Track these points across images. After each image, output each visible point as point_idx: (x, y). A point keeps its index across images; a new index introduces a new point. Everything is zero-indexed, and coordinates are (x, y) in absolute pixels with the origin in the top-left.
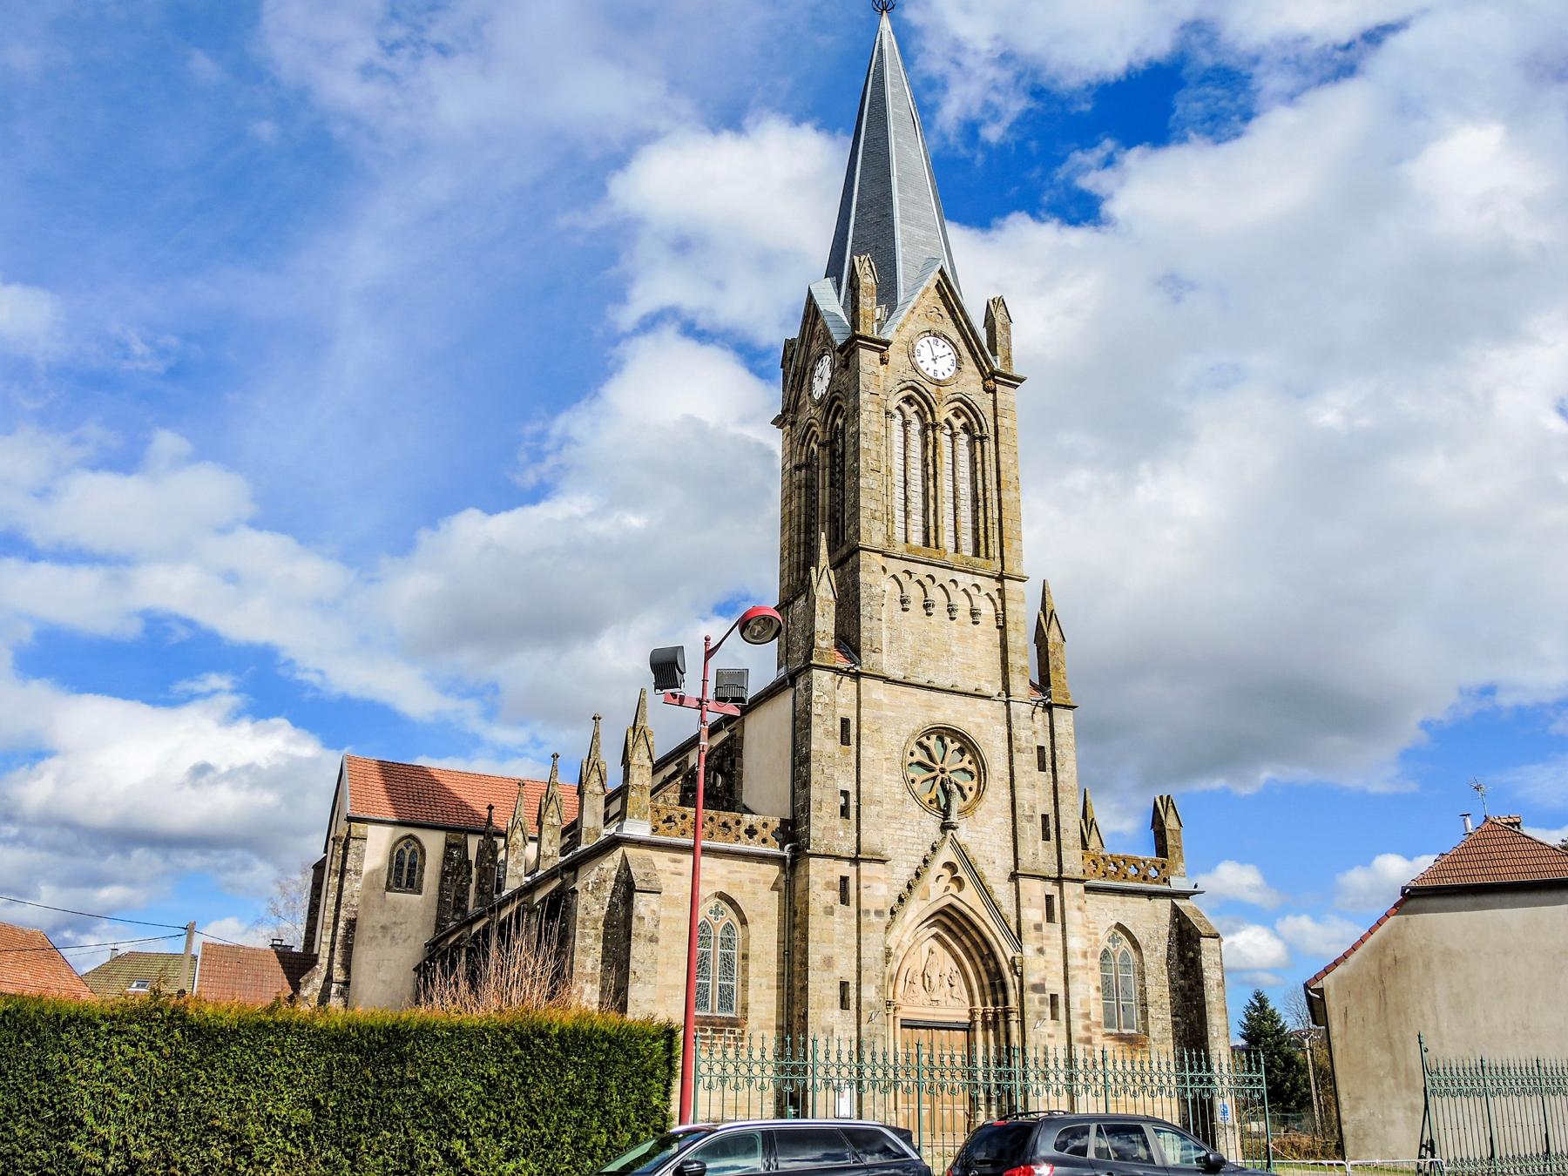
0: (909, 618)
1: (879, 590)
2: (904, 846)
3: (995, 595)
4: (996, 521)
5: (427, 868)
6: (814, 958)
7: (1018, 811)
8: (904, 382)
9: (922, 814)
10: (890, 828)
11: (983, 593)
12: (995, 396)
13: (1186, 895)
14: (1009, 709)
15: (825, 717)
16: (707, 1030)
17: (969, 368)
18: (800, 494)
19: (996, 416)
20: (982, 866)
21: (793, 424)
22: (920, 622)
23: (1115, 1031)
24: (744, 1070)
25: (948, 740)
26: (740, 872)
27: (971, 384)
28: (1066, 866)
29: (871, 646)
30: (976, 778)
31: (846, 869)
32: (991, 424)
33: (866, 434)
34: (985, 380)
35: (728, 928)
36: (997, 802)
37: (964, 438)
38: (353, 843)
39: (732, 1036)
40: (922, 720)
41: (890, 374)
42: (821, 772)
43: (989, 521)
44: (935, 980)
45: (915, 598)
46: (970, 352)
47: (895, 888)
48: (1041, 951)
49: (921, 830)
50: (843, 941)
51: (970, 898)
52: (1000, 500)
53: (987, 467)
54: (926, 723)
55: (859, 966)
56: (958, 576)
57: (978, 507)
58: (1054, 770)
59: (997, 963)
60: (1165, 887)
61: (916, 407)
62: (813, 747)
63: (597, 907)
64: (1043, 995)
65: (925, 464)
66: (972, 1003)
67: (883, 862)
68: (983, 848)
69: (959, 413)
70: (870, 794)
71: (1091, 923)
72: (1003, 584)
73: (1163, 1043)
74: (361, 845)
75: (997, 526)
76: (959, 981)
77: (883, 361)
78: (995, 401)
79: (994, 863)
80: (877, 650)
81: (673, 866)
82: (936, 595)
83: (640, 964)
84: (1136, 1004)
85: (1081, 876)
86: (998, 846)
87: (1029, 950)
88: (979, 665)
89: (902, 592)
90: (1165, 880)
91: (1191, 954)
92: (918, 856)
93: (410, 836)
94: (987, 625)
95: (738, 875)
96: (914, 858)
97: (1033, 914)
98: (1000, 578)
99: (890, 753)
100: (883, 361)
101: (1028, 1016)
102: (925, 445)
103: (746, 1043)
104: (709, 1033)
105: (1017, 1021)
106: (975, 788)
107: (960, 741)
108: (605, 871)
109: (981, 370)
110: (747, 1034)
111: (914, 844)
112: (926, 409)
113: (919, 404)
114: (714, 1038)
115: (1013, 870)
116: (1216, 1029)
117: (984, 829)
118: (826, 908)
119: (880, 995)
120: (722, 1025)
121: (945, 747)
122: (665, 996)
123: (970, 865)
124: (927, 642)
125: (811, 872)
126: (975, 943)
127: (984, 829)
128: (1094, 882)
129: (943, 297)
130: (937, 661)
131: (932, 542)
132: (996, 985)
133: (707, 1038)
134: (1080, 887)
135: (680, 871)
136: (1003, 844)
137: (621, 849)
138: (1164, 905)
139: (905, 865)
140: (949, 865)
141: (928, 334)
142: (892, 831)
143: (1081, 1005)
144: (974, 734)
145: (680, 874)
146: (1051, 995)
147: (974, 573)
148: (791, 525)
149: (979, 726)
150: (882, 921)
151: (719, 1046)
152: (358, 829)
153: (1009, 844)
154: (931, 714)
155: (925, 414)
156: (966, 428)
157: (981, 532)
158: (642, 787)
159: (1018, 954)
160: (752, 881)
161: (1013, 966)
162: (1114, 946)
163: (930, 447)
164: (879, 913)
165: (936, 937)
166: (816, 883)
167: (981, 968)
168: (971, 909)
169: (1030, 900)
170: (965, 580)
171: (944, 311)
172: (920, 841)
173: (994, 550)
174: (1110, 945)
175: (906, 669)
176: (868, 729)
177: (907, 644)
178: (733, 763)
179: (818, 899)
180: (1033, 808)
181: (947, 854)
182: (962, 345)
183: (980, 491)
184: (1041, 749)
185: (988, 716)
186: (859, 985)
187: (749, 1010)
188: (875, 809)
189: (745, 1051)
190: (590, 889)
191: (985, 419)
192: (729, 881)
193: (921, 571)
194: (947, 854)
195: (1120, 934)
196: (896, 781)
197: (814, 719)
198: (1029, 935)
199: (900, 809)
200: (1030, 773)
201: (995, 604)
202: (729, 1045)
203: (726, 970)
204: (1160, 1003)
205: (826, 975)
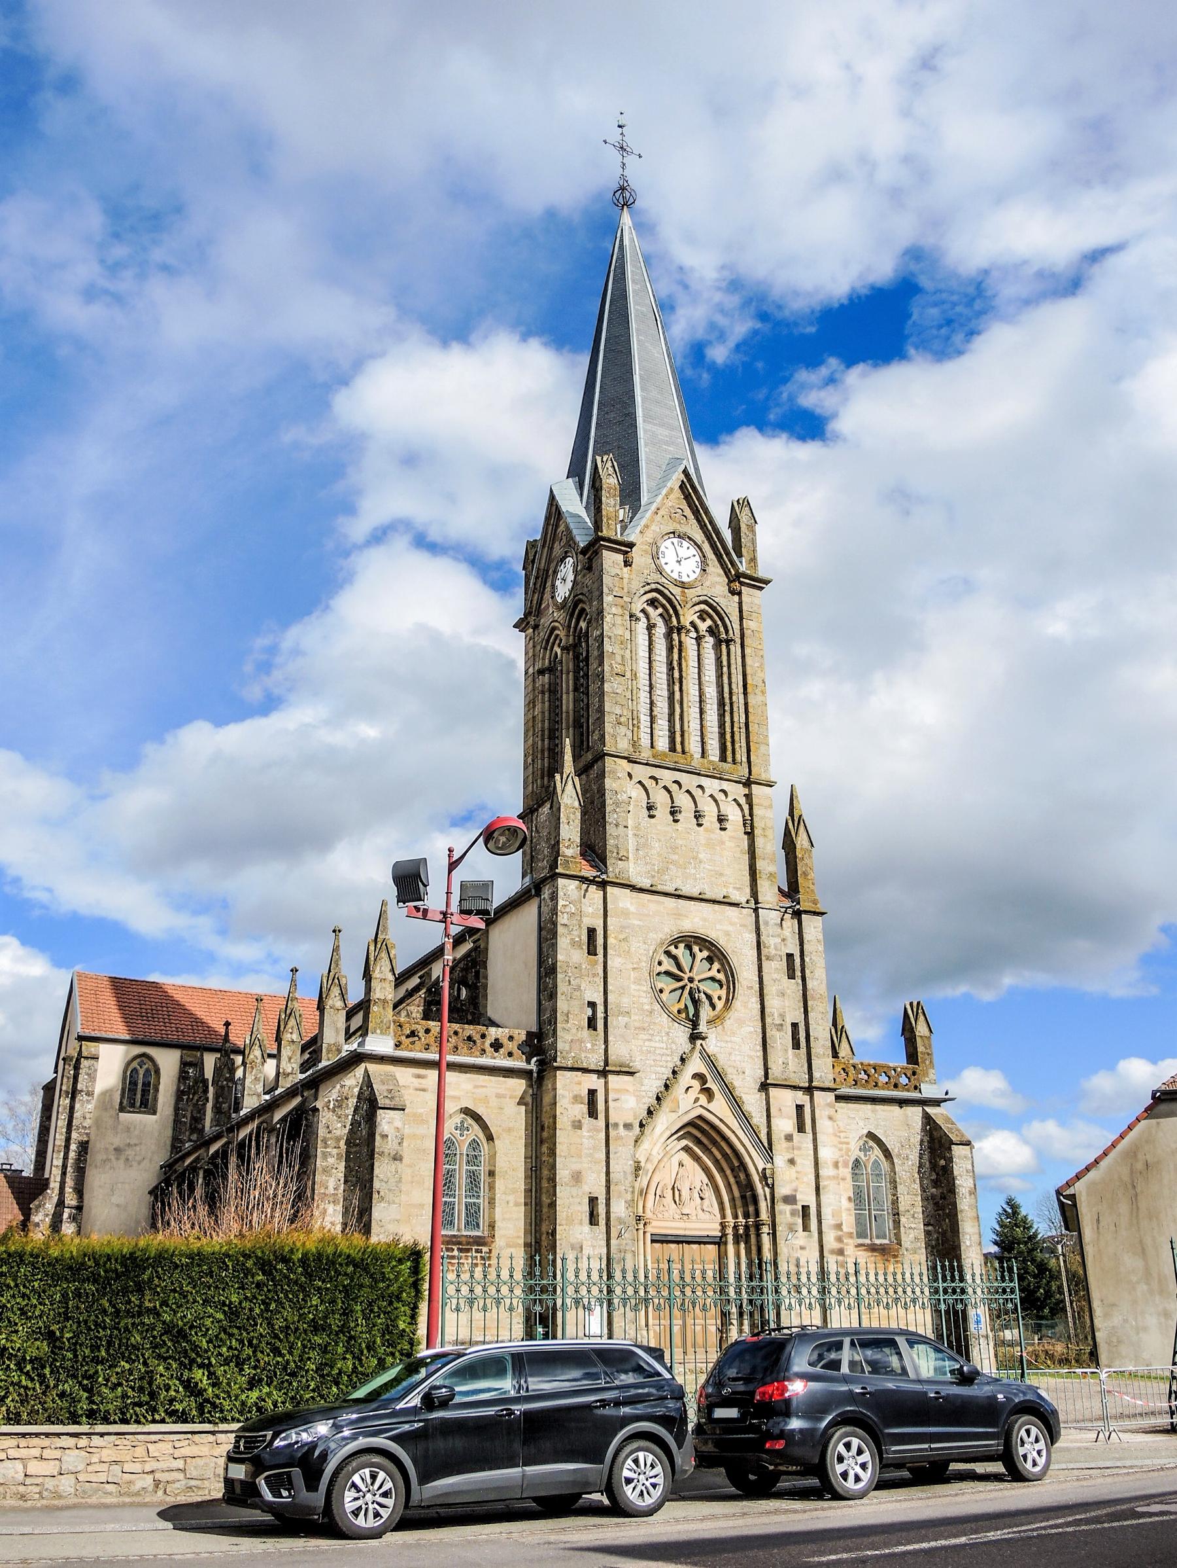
1: (625, 797)
2: (653, 1058)
3: (743, 801)
4: (743, 726)
5: (161, 1087)
6: (563, 1173)
7: (768, 1020)
8: (648, 584)
11: (730, 798)
12: (740, 598)
13: (937, 1102)
14: (757, 917)
18: (543, 699)
19: (741, 618)
20: (733, 1078)
21: (536, 627)
22: (669, 829)
25: (696, 949)
27: (716, 585)
28: (816, 1074)
30: (725, 987)
31: (594, 1082)
32: (736, 626)
33: (610, 638)
34: (730, 582)
35: (474, 1145)
37: (709, 641)
38: (84, 1063)
39: (479, 1255)
41: (633, 576)
43: (736, 725)
44: (685, 1193)
46: (715, 554)
48: (792, 1162)
50: (591, 1155)
51: (720, 1109)
52: (746, 704)
53: (733, 671)
55: (608, 1181)
56: (705, 782)
57: (724, 711)
58: (804, 979)
59: (748, 1175)
60: (915, 1095)
61: (660, 610)
62: (560, 957)
63: (339, 1125)
65: (671, 669)
66: (723, 1216)
67: (632, 1074)
68: (733, 1058)
69: (705, 616)
70: (618, 1006)
72: (750, 790)
74: (93, 1065)
75: (743, 730)
76: (709, 1194)
77: (627, 563)
78: (740, 603)
82: (683, 800)
83: (383, 1184)
84: (888, 1213)
85: (832, 1085)
87: (780, 1160)
88: (728, 871)
89: (649, 799)
90: (916, 1087)
91: (943, 1162)
93: (144, 1055)
97: (784, 1124)
98: (748, 783)
100: (627, 563)
101: (779, 1228)
102: (670, 649)
103: (494, 1262)
105: (769, 1234)
106: (724, 997)
107: (709, 949)
108: (347, 1088)
109: (727, 572)
110: (494, 1254)
112: (671, 611)
113: (663, 606)
115: (763, 1080)
118: (574, 1122)
119: (630, 1209)
120: (468, 1243)
123: (720, 1076)
124: (674, 849)
125: (559, 1085)
126: (725, 1155)
128: (845, 1090)
129: (687, 497)
131: (679, 747)
132: (746, 1197)
133: (453, 1257)
134: (831, 1096)
136: (753, 1053)
137: (363, 1065)
138: (915, 1113)
140: (699, 1077)
141: (672, 535)
144: (722, 942)
145: (424, 1090)
146: (803, 1206)
147: (721, 779)
148: (534, 730)
149: (727, 934)
152: (89, 1048)
155: (670, 616)
156: (711, 631)
157: (728, 736)
158: (385, 1001)
159: (769, 1166)
160: (498, 1096)
161: (764, 1177)
162: (865, 1156)
163: (676, 650)
164: (628, 1126)
165: (686, 1149)
167: (732, 1180)
168: (721, 1120)
170: (712, 785)
171: (688, 512)
172: (668, 1052)
173: (741, 755)
175: (653, 877)
176: (616, 938)
177: (654, 852)
178: (477, 974)
180: (782, 1016)
181: (696, 1065)
182: (706, 547)
183: (726, 695)
184: (790, 956)
186: (608, 1200)
187: (496, 1228)
188: (622, 1020)
190: (331, 1106)
193: (667, 776)
194: (696, 1065)
195: (871, 1143)
197: (560, 930)
198: (780, 1146)
199: (648, 1019)
201: (742, 810)
205: (574, 1191)
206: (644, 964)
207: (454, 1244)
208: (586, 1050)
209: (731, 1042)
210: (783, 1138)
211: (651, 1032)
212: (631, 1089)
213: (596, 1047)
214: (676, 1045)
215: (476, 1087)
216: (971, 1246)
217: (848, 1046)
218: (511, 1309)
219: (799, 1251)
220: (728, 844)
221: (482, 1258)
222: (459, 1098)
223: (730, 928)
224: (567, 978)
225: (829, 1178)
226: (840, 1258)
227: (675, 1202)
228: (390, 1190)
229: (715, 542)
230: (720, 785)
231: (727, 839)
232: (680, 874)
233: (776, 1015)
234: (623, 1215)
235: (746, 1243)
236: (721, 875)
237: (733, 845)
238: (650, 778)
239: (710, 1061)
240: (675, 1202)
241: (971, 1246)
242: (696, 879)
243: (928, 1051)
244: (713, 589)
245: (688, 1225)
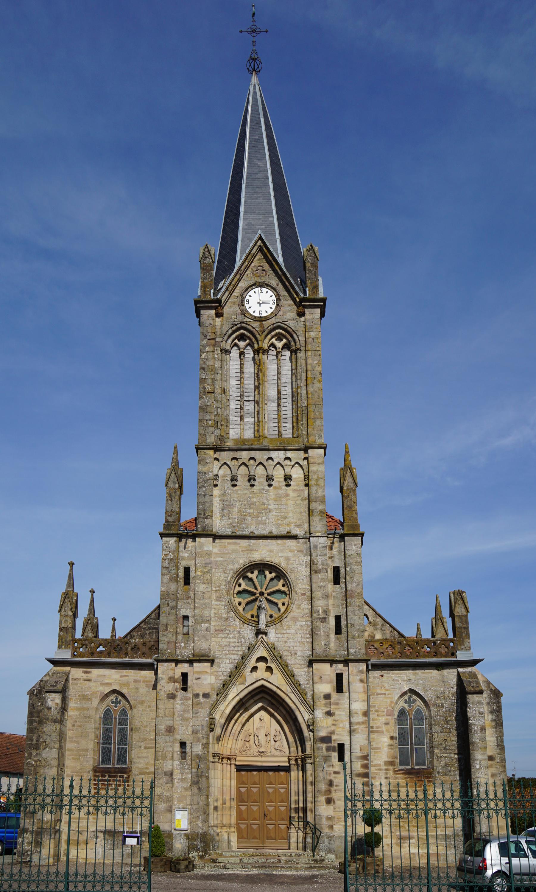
0: (236, 491)
2: (228, 649)
8: (236, 325)
9: (242, 625)
10: (217, 638)
15: (170, 568)
16: (106, 776)
17: (285, 302)
22: (247, 492)
23: (409, 767)
24: (492, 805)
25: (249, 575)
26: (127, 676)
29: (204, 514)
36: (300, 611)
39: (121, 779)
40: (243, 561)
41: (224, 322)
45: (242, 476)
47: (220, 678)
48: (329, 714)
49: (241, 637)
50: (182, 715)
54: (246, 562)
63: (39, 704)
64: (330, 744)
68: (288, 644)
69: (282, 337)
71: (387, 690)
73: (446, 775)
77: (219, 315)
79: (296, 654)
80: (209, 517)
81: (85, 676)
83: (48, 737)
84: (427, 747)
85: (365, 657)
86: (299, 642)
87: (319, 713)
88: (290, 515)
92: (237, 654)
94: (297, 486)
95: (126, 678)
96: (235, 656)
99: (219, 587)
103: (131, 783)
104: (106, 778)
110: (131, 779)
111: (235, 646)
114: (110, 781)
116: (478, 762)
117: (289, 631)
118: (168, 694)
119: (205, 749)
120: (115, 772)
121: (251, 580)
122: (80, 756)
124: (250, 505)
127: (289, 631)
128: (374, 660)
130: (258, 518)
133: (105, 781)
134: (363, 667)
135: (89, 678)
139: (228, 661)
142: (220, 640)
143: (361, 750)
145: (89, 680)
146: (339, 744)
147: (285, 450)
149: (287, 558)
150: (208, 700)
151: (113, 785)
153: (308, 640)
154: (251, 555)
156: (286, 346)
159: (311, 717)
160: (135, 681)
162: (410, 706)
166: (162, 679)
168: (278, 688)
169: (321, 678)
172: (239, 644)
174: (407, 707)
175: (234, 526)
176: (201, 572)
177: (235, 510)
179: (163, 689)
182: (280, 288)
185: (294, 551)
189: (130, 789)
190: (35, 693)
191: (298, 336)
192: (121, 682)
196: (223, 605)
199: (225, 624)
200: (324, 587)
202: (120, 785)
203: (122, 739)
204: (444, 745)
205: (168, 738)
207: (106, 773)
208: (181, 648)
210: (322, 697)
211: (227, 632)
213: (187, 645)
214: (245, 639)
215: (121, 677)
216: (480, 768)
217: (443, 630)
218: (142, 815)
219: (334, 775)
220: (292, 495)
221: (123, 781)
222: (111, 684)
223: (290, 554)
224: (167, 602)
225: (358, 723)
226: (366, 779)
228: (52, 740)
229: (284, 282)
230: (285, 454)
231: (291, 492)
232: (254, 522)
233: (321, 611)
234: (201, 753)
235: (303, 770)
236: (286, 517)
237: (295, 495)
238: (249, 460)
239: (272, 648)
241: (480, 768)
242: (266, 524)
243: (465, 626)
244: (285, 317)
245: (264, 759)
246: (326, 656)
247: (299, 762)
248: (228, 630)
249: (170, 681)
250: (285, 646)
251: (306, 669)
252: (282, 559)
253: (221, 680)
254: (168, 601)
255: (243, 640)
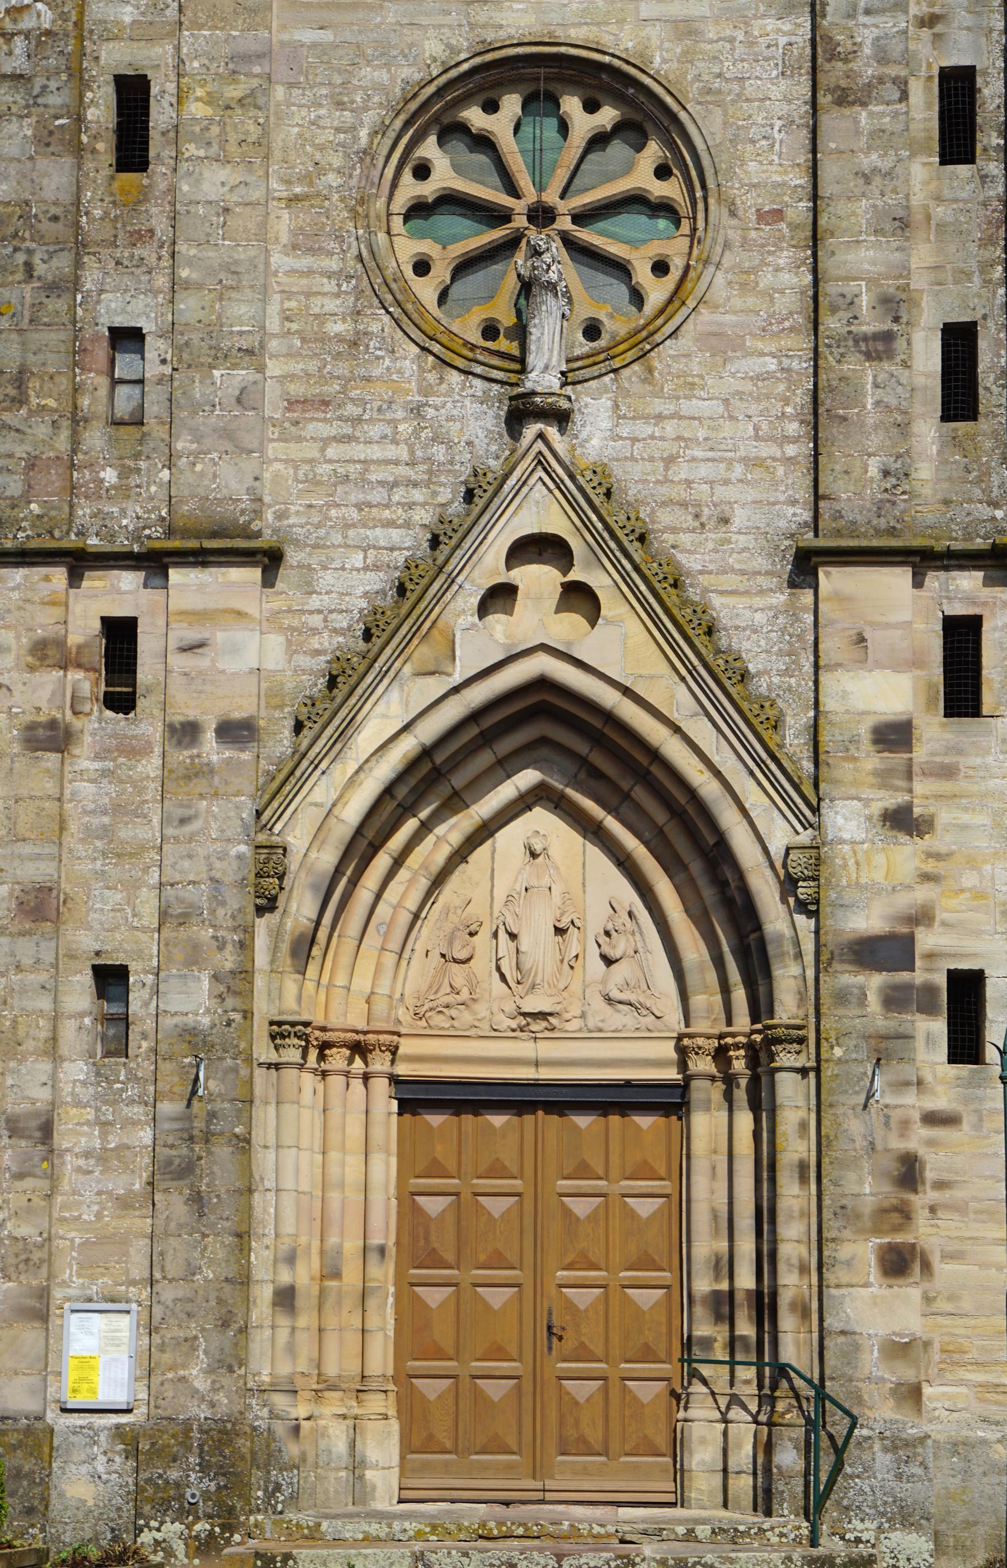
42: (19, 276)
50: (106, 832)
68: (682, 472)
79: (725, 521)
92: (407, 525)
107: (619, 99)
118: (31, 727)
119: (230, 1002)
139: (357, 559)
159: (805, 837)
168: (627, 692)
169: (861, 639)
172: (417, 473)
176: (210, 100)
199: (342, 368)
206: (333, 179)
208: (98, 491)
209: (676, 416)
211: (351, 410)
212: (252, 609)
213: (134, 480)
214: (450, 445)
219: (926, 1132)
224: (21, 258)
227: (503, 978)
234: (206, 1021)
240: (503, 978)
245: (547, 1050)
246: (892, 532)
247: (739, 1065)
248: (362, 402)
249: (43, 658)
250: (666, 481)
251: (781, 598)
252: (654, 33)
253: (318, 653)
254: (30, 252)
255: (439, 452)
